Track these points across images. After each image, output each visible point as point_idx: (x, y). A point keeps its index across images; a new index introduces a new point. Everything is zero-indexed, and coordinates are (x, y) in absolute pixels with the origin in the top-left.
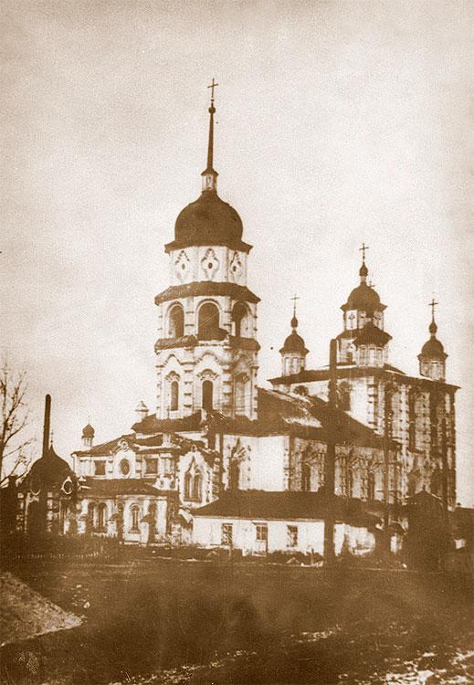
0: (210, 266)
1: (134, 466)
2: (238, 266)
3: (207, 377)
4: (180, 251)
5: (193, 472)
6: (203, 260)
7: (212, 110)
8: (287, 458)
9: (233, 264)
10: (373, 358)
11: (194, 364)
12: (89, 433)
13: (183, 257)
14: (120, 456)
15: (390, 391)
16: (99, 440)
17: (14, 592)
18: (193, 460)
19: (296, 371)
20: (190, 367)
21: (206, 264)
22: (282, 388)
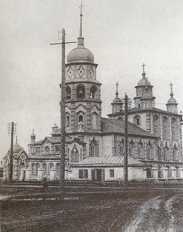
0: (81, 72)
1: (51, 148)
2: (83, 71)
3: (81, 114)
4: (69, 67)
5: (75, 150)
6: (78, 70)
7: (81, 15)
8: (114, 144)
9: (90, 71)
10: (146, 106)
11: (75, 109)
12: (33, 137)
13: (71, 70)
14: (46, 145)
15: (156, 118)
16: (37, 140)
17: (1, 178)
18: (75, 145)
19: (118, 111)
20: (74, 110)
21: (79, 72)
22: (113, 118)
